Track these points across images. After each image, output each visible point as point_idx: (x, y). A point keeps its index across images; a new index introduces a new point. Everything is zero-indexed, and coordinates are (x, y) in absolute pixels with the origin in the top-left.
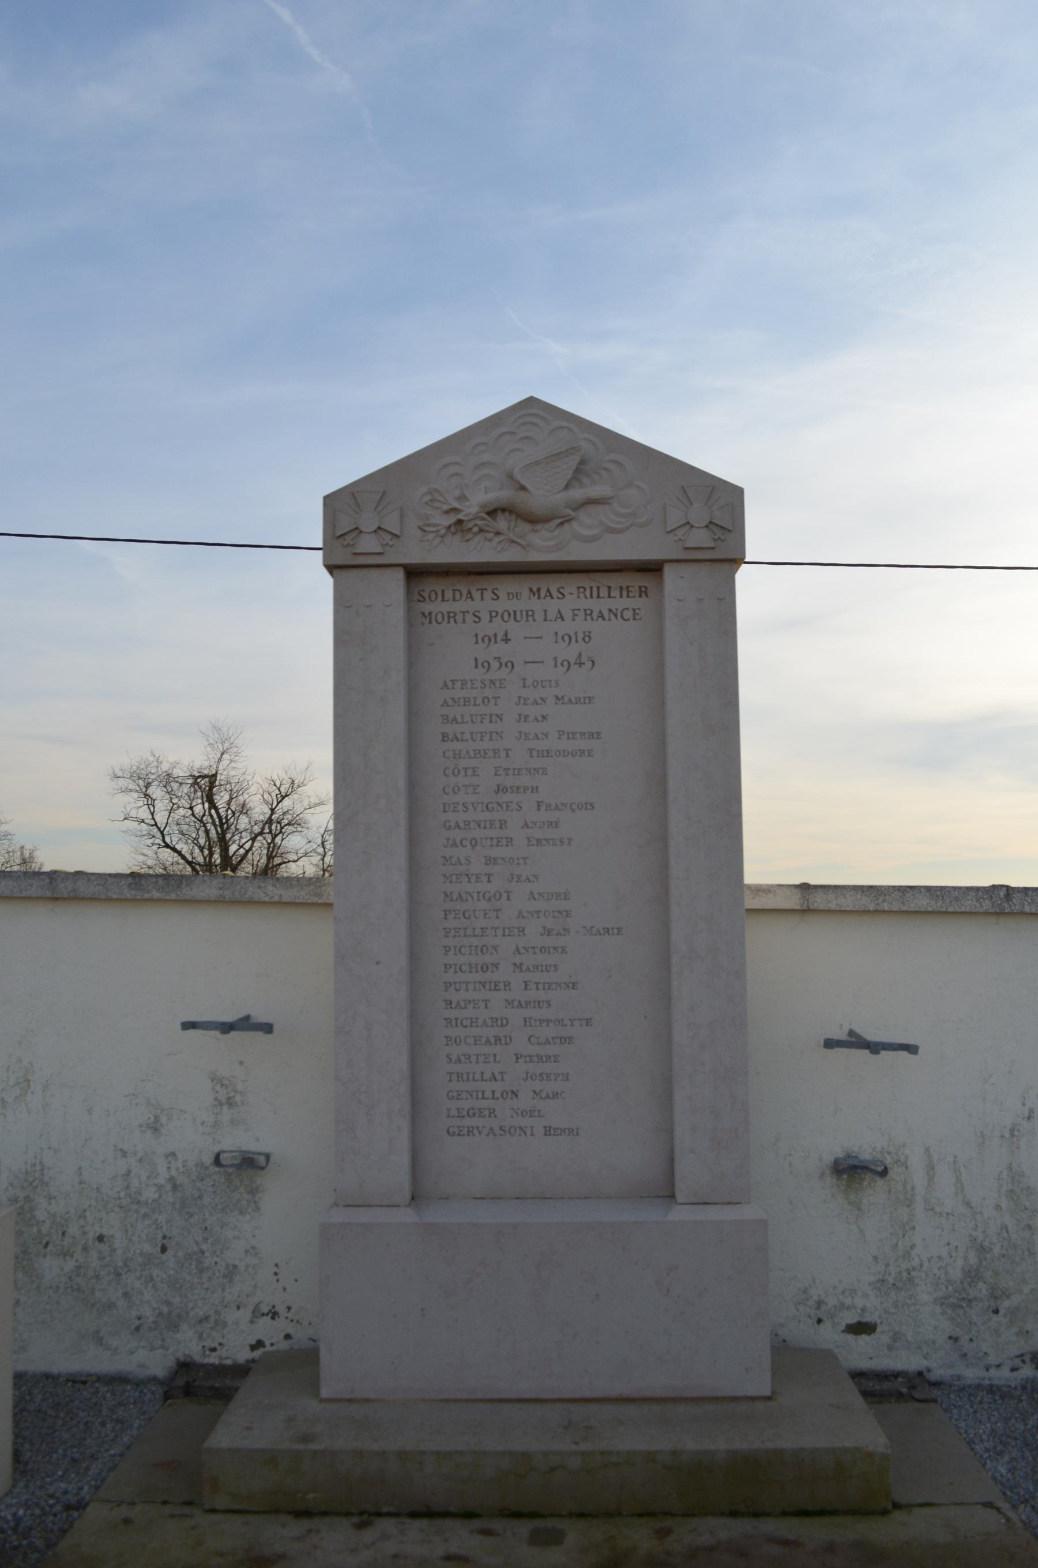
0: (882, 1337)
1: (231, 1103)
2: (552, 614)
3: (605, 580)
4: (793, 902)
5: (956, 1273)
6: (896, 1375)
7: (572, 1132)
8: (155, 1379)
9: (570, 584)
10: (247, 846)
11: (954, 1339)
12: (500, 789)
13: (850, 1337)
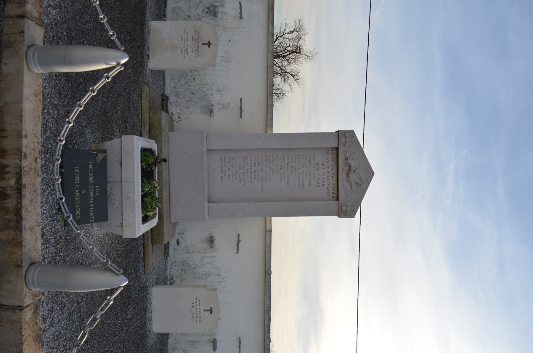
0: (176, 246)
1: (224, 107)
2: (328, 178)
4: (268, 228)
5: (189, 262)
6: (168, 249)
7: (222, 182)
8: (164, 92)
9: (335, 182)
10: (277, 65)
11: (176, 262)
12: (292, 167)
13: (176, 240)
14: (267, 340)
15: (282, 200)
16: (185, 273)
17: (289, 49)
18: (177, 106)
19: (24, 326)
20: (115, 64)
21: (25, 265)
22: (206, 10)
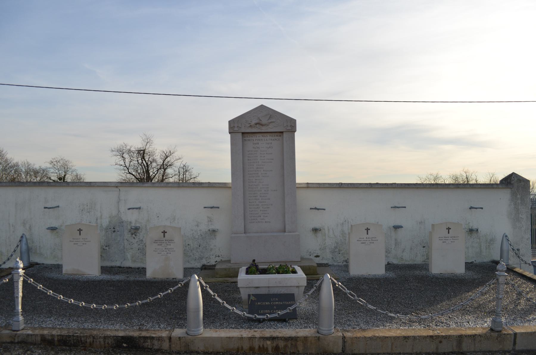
0: (320, 258)
1: (211, 221)
3: (274, 134)
4: (306, 186)
5: (333, 247)
7: (269, 222)
9: (268, 135)
14: (394, 186)
15: (283, 175)
17: (140, 161)
19: (355, 336)
20: (198, 282)
21: (318, 335)
22: (134, 235)
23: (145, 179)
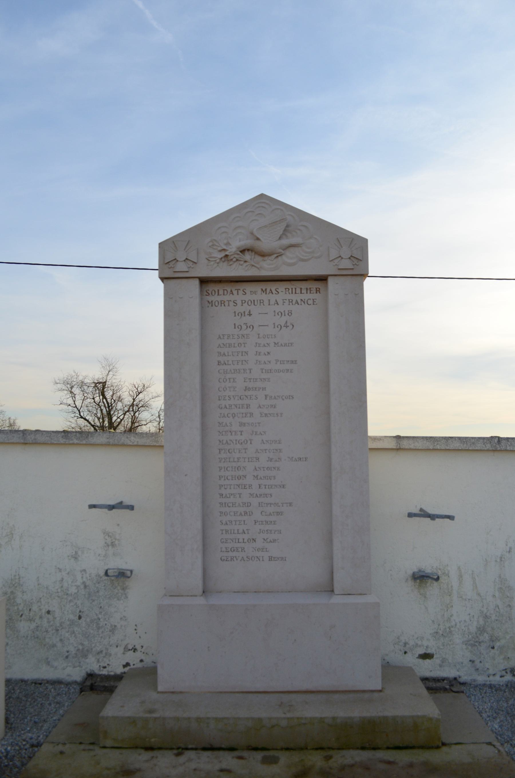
0: (436, 660)
1: (113, 545)
2: (273, 302)
4: (392, 445)
5: (473, 629)
6: (443, 679)
8: (76, 682)
9: (282, 287)
10: (121, 417)
11: (472, 661)
12: (246, 389)
13: (421, 660)
16: (498, 639)
18: (108, 655)
23: (107, 423)
